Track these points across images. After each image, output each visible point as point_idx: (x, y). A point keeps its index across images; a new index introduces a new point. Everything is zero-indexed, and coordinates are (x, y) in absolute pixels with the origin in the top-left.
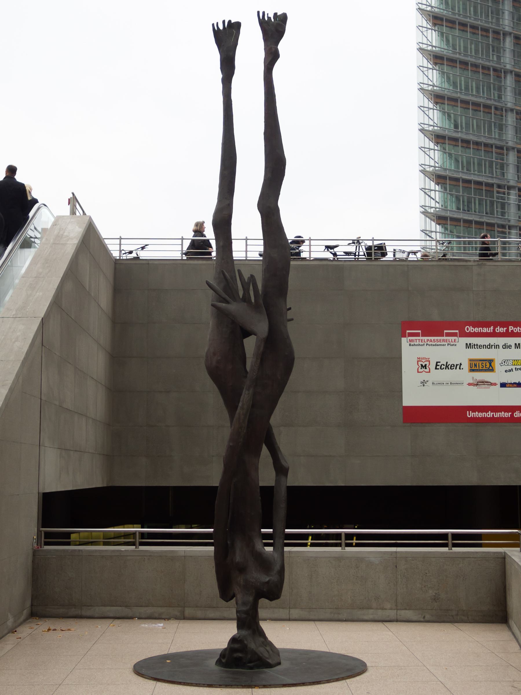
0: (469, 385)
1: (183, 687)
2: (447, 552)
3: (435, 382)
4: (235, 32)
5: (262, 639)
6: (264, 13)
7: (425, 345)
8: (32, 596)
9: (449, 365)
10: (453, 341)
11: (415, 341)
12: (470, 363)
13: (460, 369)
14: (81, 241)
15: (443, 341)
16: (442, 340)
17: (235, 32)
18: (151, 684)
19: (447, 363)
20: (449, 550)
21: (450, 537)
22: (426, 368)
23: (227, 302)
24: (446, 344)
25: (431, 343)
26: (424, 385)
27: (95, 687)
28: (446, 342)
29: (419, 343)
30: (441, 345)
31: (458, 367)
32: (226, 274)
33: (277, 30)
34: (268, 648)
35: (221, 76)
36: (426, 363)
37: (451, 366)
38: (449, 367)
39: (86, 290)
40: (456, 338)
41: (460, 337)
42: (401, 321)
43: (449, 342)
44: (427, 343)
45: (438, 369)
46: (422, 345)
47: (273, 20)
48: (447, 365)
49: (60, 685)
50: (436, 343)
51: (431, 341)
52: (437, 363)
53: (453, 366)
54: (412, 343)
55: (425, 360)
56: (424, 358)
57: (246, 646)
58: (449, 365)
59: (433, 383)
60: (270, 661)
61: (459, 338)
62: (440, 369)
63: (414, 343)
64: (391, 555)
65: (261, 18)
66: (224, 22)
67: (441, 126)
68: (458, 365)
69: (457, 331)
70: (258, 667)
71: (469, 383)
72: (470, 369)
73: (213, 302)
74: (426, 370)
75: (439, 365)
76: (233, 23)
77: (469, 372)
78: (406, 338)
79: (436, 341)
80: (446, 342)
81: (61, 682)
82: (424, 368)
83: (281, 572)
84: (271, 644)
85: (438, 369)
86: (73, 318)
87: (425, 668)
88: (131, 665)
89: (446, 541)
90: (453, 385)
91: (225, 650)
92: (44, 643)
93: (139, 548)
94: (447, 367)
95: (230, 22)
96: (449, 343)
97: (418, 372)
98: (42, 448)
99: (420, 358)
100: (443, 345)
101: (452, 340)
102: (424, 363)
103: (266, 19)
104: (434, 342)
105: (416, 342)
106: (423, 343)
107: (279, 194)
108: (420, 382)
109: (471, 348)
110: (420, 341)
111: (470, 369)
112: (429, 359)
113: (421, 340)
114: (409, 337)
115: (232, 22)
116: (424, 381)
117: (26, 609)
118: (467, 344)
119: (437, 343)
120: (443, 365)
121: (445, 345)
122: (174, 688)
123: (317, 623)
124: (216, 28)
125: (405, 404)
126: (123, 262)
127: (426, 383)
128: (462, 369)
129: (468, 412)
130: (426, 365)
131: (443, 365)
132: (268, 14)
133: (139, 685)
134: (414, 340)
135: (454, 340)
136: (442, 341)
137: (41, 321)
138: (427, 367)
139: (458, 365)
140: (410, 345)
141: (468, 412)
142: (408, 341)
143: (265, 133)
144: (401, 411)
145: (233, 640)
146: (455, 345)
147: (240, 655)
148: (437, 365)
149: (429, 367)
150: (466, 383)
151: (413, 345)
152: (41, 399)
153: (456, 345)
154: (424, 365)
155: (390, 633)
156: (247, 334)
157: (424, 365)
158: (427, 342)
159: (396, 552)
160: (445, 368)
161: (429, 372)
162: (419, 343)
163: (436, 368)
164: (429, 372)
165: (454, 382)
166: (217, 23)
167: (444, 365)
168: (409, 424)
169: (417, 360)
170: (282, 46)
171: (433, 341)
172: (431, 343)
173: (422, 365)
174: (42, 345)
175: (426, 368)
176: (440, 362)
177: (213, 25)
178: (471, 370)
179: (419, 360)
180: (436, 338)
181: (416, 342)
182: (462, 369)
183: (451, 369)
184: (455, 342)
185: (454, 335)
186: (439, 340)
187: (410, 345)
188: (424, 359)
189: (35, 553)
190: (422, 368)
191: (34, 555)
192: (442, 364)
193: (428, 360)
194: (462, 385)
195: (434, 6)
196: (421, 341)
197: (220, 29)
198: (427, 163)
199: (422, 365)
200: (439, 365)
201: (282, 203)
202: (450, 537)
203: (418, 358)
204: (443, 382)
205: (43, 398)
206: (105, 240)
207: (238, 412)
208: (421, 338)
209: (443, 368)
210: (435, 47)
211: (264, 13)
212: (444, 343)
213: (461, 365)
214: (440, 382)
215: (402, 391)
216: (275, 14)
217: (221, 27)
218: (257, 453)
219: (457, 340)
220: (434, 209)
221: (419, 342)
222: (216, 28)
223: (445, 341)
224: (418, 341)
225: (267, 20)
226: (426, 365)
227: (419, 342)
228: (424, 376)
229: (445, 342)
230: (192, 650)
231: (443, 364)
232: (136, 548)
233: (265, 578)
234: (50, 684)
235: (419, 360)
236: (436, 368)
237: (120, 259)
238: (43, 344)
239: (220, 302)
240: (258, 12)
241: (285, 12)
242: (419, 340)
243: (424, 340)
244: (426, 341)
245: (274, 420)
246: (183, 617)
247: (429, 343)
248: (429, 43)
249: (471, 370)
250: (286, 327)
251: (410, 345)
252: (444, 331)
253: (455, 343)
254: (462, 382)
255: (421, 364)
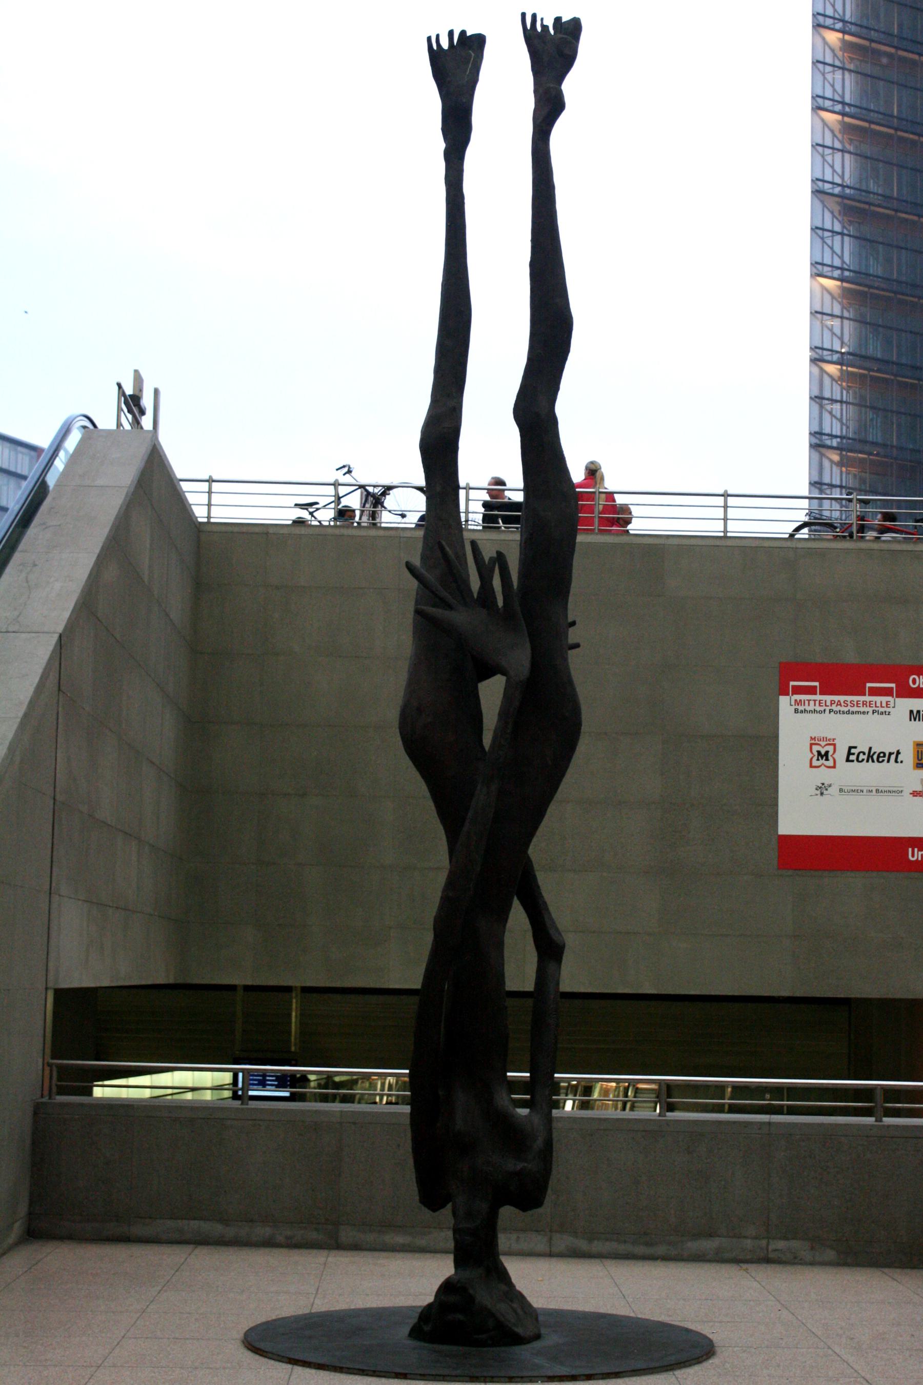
0: (914, 796)
1: (347, 1377)
2: (872, 1125)
3: (846, 789)
4: (473, 55)
5: (504, 1287)
6: (534, 16)
7: (827, 711)
8: (31, 1195)
9: (875, 753)
10: (883, 705)
11: (807, 703)
12: (916, 750)
13: (896, 761)
14: (136, 482)
15: (863, 704)
16: (861, 703)
17: (473, 55)
18: (283, 1369)
19: (870, 748)
20: (876, 1121)
21: (879, 1096)
22: (827, 759)
23: (450, 607)
24: (871, 710)
25: (839, 708)
26: (822, 794)
27: (170, 1373)
28: (870, 706)
29: (815, 707)
30: (858, 712)
31: (893, 757)
32: (448, 549)
33: (561, 54)
34: (515, 1305)
35: (442, 145)
36: (827, 748)
37: (879, 757)
38: (875, 757)
39: (144, 581)
40: (889, 698)
41: (898, 696)
42: (781, 663)
43: (876, 707)
44: (830, 708)
45: (853, 761)
46: (820, 712)
47: (552, 32)
48: (872, 753)
49: (99, 1367)
50: (849, 708)
51: (839, 704)
52: (850, 748)
53: (882, 755)
54: (801, 708)
55: (825, 743)
56: (823, 738)
57: (472, 1299)
58: (875, 753)
59: (841, 790)
60: (519, 1330)
61: (897, 699)
62: (855, 761)
63: (804, 707)
64: (760, 1129)
65: (529, 27)
66: (451, 33)
67: (857, 269)
68: (893, 753)
69: (893, 685)
70: (496, 1343)
71: (914, 791)
72: (917, 764)
73: (419, 607)
74: (827, 763)
75: (853, 754)
76: (471, 36)
77: (914, 769)
78: (788, 697)
79: (849, 704)
80: (870, 706)
81: (100, 1362)
82: (824, 758)
83: (547, 1151)
84: (521, 1297)
85: (853, 761)
86: (118, 636)
87: (830, 1352)
88: (238, 1334)
89: (871, 1103)
90: (882, 794)
91: (430, 1306)
92: (59, 1288)
93: (247, 1104)
94: (870, 757)
95: (463, 33)
96: (877, 709)
97: (811, 766)
98: (55, 898)
99: (815, 738)
100: (864, 713)
101: (881, 702)
102: (823, 747)
103: (539, 29)
104: (844, 706)
105: (809, 705)
106: (822, 709)
107: (557, 389)
108: (815, 787)
109: (919, 720)
110: (817, 703)
111: (917, 764)
112: (834, 740)
113: (820, 701)
114: (794, 696)
115: (468, 34)
116: (823, 784)
117: (19, 1220)
118: (911, 712)
119: (852, 709)
120: (861, 754)
121: (868, 712)
122: (328, 1378)
123: (609, 1263)
124: (435, 47)
125: (785, 828)
126: (215, 529)
127: (827, 790)
128: (902, 762)
129: (910, 850)
130: (827, 752)
131: (861, 754)
132: (542, 19)
133: (259, 1372)
134: (804, 701)
135: (887, 702)
136: (861, 705)
137: (57, 641)
138: (830, 758)
139: (893, 753)
140: (795, 711)
141: (910, 850)
142: (793, 703)
143: (532, 265)
144: (774, 843)
145: (447, 1287)
146: (887, 713)
147: (460, 1317)
148: (849, 753)
149: (834, 756)
150: (907, 792)
151: (802, 712)
152: (54, 799)
153: (889, 712)
154: (823, 753)
155: (755, 1284)
156: (487, 671)
157: (823, 753)
158: (831, 706)
159: (769, 1123)
160: (865, 760)
161: (834, 767)
162: (815, 707)
163: (848, 760)
164: (834, 767)
165: (883, 789)
166: (438, 36)
167: (864, 754)
168: (790, 872)
169: (808, 742)
170: (570, 86)
171: (843, 704)
172: (839, 708)
173: (819, 753)
174: (59, 690)
175: (827, 759)
176: (855, 747)
177: (429, 39)
178: (920, 764)
179: (814, 741)
180: (849, 698)
181: (809, 705)
182: (902, 762)
183: (878, 761)
184: (887, 707)
185: (887, 692)
186: (855, 703)
187: (796, 711)
188: (823, 740)
189: (38, 1109)
190: (820, 758)
191: (35, 1113)
192: (862, 752)
193: (832, 742)
194: (900, 794)
195: (850, 20)
196: (820, 703)
197: (444, 49)
198: (827, 345)
199: (819, 753)
200: (853, 754)
201: (563, 407)
202: (879, 1096)
203: (811, 737)
204: (862, 788)
205: (58, 797)
206: (181, 483)
207: (465, 829)
208: (818, 697)
209: (863, 760)
210: (849, 105)
211: (534, 16)
212: (865, 709)
213: (900, 753)
214: (856, 788)
215: (777, 805)
216: (558, 20)
217: (445, 45)
218: (503, 915)
219: (892, 705)
220: (839, 440)
221: (815, 705)
222: (435, 47)
223: (868, 704)
224: (812, 703)
225: (542, 30)
226: (827, 752)
227: (815, 705)
228: (823, 775)
229: (867, 706)
230: (358, 1306)
231: (863, 750)
232: (242, 1104)
233: (513, 1165)
234: (79, 1364)
235: (814, 741)
236: (848, 760)
237: (209, 523)
238: (63, 688)
239: (435, 606)
240: (523, 15)
241: (577, 16)
242: (815, 701)
243: (826, 701)
244: (828, 703)
245: (537, 850)
246: (336, 1245)
247: (834, 707)
248: (837, 98)
249: (919, 766)
250: (565, 659)
251: (796, 711)
252: (866, 685)
253: (888, 710)
254: (900, 789)
255: (819, 750)
